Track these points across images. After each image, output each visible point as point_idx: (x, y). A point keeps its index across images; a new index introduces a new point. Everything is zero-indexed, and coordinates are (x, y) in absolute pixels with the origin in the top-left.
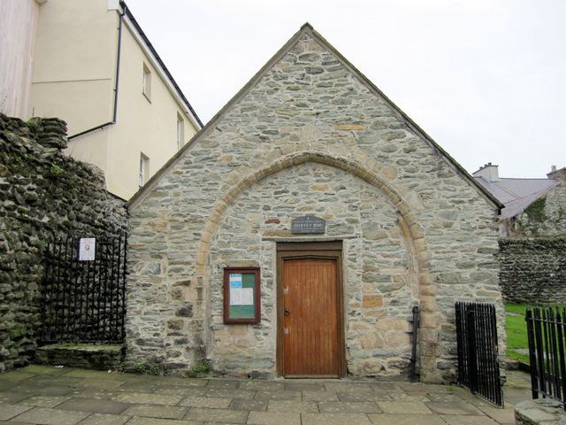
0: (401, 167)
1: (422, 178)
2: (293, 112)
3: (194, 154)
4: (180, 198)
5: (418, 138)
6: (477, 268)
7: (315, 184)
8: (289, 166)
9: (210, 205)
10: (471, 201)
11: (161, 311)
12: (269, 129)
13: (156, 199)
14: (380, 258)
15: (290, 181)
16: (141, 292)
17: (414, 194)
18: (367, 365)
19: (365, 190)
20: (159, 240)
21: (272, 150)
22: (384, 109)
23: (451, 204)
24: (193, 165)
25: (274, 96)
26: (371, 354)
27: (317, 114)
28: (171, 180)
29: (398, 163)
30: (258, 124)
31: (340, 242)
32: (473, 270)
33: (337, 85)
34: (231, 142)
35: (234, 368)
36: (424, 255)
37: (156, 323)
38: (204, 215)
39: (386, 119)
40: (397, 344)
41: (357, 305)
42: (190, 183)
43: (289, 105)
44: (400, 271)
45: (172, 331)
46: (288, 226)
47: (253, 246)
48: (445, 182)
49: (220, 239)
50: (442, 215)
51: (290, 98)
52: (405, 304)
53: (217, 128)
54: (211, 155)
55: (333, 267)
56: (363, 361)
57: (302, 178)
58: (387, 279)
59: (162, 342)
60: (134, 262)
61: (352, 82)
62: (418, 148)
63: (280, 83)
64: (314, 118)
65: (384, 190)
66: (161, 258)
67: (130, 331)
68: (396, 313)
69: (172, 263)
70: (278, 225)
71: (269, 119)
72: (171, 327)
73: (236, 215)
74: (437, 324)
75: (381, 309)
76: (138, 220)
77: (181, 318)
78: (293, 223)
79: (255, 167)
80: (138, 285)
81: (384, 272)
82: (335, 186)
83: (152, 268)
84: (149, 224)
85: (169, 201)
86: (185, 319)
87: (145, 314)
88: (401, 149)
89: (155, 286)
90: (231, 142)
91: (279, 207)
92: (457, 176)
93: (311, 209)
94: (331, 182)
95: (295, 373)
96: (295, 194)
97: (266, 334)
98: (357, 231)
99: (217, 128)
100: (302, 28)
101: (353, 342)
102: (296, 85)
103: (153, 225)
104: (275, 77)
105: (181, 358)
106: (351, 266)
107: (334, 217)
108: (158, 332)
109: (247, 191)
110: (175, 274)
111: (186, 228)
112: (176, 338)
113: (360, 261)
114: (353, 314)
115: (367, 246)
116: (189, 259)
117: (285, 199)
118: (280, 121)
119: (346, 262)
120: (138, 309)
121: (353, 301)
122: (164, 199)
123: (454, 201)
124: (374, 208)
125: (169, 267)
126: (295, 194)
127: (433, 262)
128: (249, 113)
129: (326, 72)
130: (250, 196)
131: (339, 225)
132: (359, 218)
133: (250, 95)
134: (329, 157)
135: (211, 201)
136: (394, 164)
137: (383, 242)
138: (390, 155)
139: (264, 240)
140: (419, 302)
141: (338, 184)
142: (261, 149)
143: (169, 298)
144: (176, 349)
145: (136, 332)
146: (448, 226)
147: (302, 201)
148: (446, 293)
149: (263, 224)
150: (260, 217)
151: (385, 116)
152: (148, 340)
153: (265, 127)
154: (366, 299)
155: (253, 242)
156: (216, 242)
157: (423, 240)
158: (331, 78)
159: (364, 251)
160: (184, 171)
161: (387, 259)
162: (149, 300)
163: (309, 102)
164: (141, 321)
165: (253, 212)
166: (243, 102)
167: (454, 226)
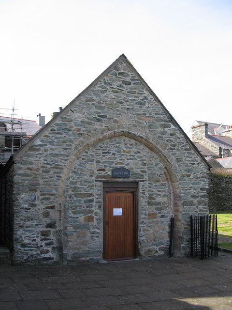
1: (177, 150)
3: (57, 125)
10: (198, 164)
11: (36, 225)
12: (102, 114)
14: (156, 192)
25: (105, 95)
29: (167, 141)
31: (137, 183)
32: (198, 199)
33: (139, 93)
34: (80, 120)
39: (162, 116)
40: (163, 238)
41: (145, 218)
44: (165, 199)
45: (43, 237)
46: (110, 173)
49: (71, 179)
54: (67, 127)
57: (117, 145)
58: (159, 204)
63: (108, 87)
64: (126, 111)
67: (16, 239)
69: (44, 194)
71: (102, 108)
76: (20, 165)
77: (49, 229)
78: (113, 171)
81: (158, 199)
91: (106, 162)
93: (122, 163)
97: (97, 237)
98: (146, 177)
104: (105, 83)
105: (50, 254)
108: (35, 238)
110: (45, 202)
111: (51, 172)
112: (46, 241)
113: (147, 194)
115: (151, 186)
116: (54, 192)
117: (109, 157)
119: (140, 195)
121: (143, 216)
123: (191, 163)
127: (182, 195)
128: (90, 103)
137: (158, 184)
138: (164, 136)
139: (96, 181)
142: (97, 126)
144: (46, 248)
146: (188, 176)
147: (118, 159)
149: (96, 171)
150: (94, 167)
152: (28, 244)
154: (150, 215)
157: (177, 183)
158: (135, 89)
160: (51, 135)
161: (160, 193)
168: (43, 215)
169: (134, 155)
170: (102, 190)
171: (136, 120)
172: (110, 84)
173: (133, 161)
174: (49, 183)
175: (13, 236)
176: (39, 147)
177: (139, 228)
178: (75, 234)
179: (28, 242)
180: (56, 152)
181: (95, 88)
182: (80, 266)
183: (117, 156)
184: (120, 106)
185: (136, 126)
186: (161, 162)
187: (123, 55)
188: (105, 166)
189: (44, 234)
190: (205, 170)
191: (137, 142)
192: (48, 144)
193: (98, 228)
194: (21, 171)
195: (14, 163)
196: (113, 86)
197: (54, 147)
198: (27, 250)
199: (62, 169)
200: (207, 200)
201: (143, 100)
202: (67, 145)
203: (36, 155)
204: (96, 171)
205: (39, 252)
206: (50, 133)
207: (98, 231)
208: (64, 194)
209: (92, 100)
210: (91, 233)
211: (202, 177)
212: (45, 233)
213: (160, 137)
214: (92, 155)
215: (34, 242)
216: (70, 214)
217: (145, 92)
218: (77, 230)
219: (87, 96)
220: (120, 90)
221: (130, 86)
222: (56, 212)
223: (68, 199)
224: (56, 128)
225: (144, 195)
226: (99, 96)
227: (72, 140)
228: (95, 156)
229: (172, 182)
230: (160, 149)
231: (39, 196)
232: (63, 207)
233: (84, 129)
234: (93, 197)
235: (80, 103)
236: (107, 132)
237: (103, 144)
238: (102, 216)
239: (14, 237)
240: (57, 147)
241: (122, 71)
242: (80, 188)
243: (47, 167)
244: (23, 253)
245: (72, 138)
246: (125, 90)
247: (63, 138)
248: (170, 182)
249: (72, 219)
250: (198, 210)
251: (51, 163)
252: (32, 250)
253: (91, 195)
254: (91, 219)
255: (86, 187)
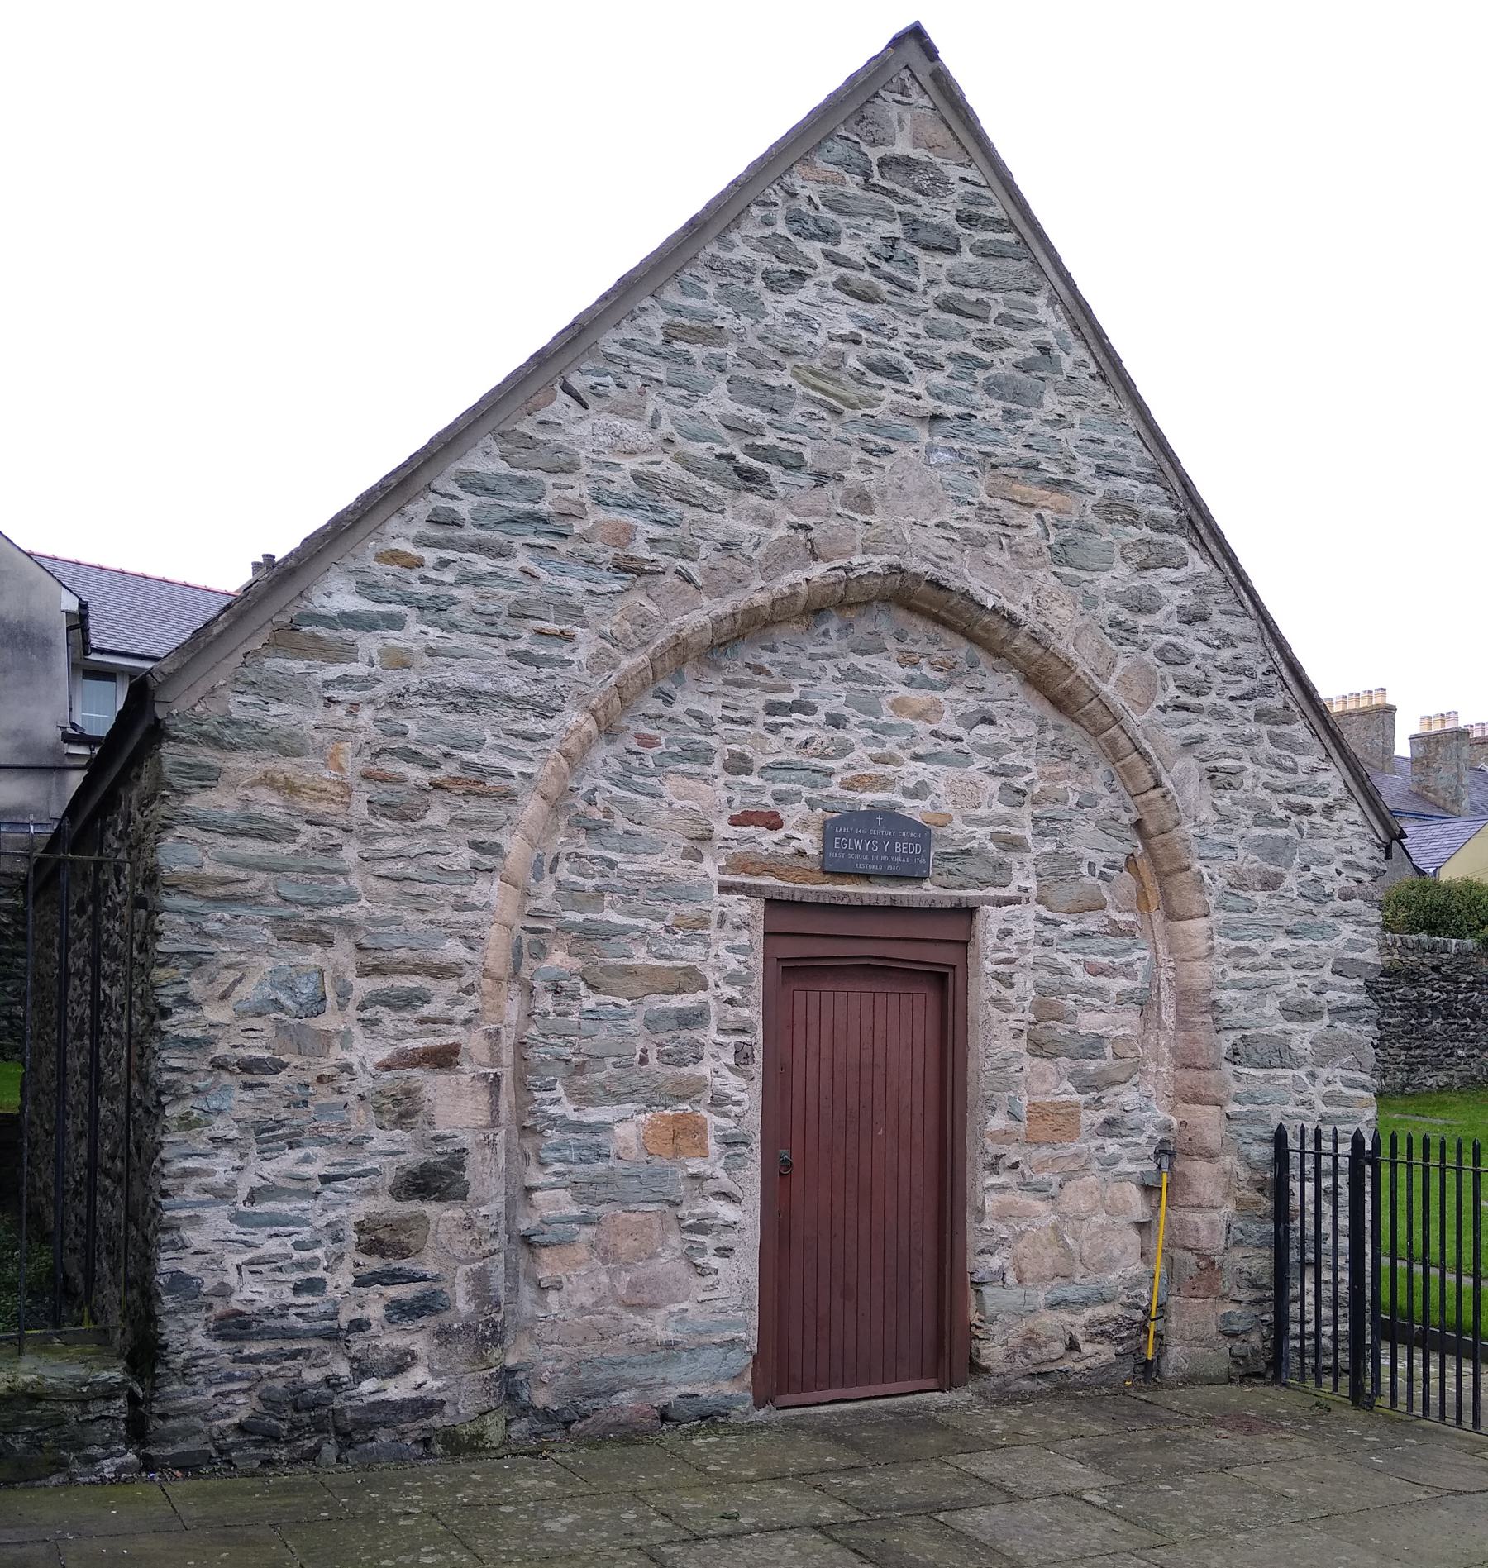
0: (1166, 670)
1: (1217, 714)
2: (854, 392)
3: (472, 484)
4: (413, 679)
5: (1218, 577)
6: (1327, 1019)
7: (903, 691)
8: (815, 609)
9: (541, 727)
10: (1328, 810)
11: (326, 1179)
12: (770, 439)
13: (298, 666)
14: (1080, 976)
15: (823, 670)
16: (238, 1103)
17: (1187, 765)
18: (1031, 1340)
19: (1050, 735)
20: (316, 860)
21: (781, 531)
22: (1136, 455)
23: (1281, 814)
24: (470, 532)
25: (790, 302)
26: (1041, 1298)
27: (936, 418)
28: (367, 588)
29: (1161, 654)
30: (732, 408)
31: (967, 912)
32: (1317, 1027)
33: (1003, 320)
34: (630, 464)
35: (612, 1392)
36: (1200, 974)
37: (306, 1234)
38: (517, 767)
39: (1140, 489)
40: (1111, 1262)
41: (1006, 1136)
42: (456, 614)
43: (842, 357)
44: (1126, 1024)
45: (374, 1264)
46: (809, 840)
47: (687, 909)
48: (1275, 740)
49: (564, 872)
50: (1258, 846)
51: (847, 327)
52: (1138, 1129)
53: (567, 389)
54: (544, 507)
55: (932, 996)
56: (1022, 1327)
57: (860, 662)
58: (1095, 1046)
59: (334, 1316)
60: (196, 961)
61: (1052, 322)
62: (1216, 616)
63: (812, 249)
64: (922, 434)
65: (1112, 743)
66: (326, 942)
67: (180, 1281)
68: (1114, 1161)
69: (378, 970)
70: (778, 835)
71: (772, 400)
72: (373, 1247)
73: (622, 781)
74: (1226, 1195)
75: (1075, 1148)
76: (208, 756)
77: (414, 1206)
78: (828, 832)
79: (718, 592)
80: (219, 1065)
81: (1090, 1022)
82: (962, 708)
83: (290, 988)
84: (268, 781)
85: (365, 683)
86: (431, 1209)
87: (252, 1198)
88: (1171, 607)
89: (298, 1068)
90: (630, 464)
91: (786, 767)
92: (1299, 724)
93: (885, 784)
94: (953, 693)
95: (804, 1388)
96: (836, 721)
97: (724, 1252)
98: (1022, 879)
99: (567, 389)
100: (897, 42)
101: (995, 1262)
102: (866, 276)
103: (289, 788)
104: (795, 218)
105: (418, 1374)
106: (998, 1002)
107: (957, 822)
108: (318, 1273)
109: (666, 685)
110: (390, 1020)
111: (437, 816)
112: (394, 1292)
113: (1025, 983)
114: (993, 1168)
115: (1047, 934)
116: (454, 951)
117: (801, 735)
118: (811, 416)
119: (982, 990)
120: (220, 1179)
121: (997, 1122)
122: (335, 671)
123: (1291, 807)
124: (1074, 799)
125: (363, 987)
126: (836, 721)
127: (1224, 997)
128: (697, 352)
129: (968, 257)
130: (677, 709)
131: (967, 853)
132: (1027, 833)
133: (703, 272)
134: (966, 595)
135: (545, 712)
136: (1149, 656)
137: (1091, 923)
138: (1143, 621)
139: (725, 888)
140: (1175, 1122)
141: (972, 703)
142: (736, 518)
143: (361, 1119)
144: (393, 1340)
145: (210, 1283)
146: (1270, 883)
147: (860, 753)
148: (1252, 1098)
149: (722, 829)
150: (713, 795)
151: (1138, 477)
152: (268, 1313)
153: (758, 430)
154: (1038, 1112)
155: (687, 895)
156: (548, 888)
157: (1202, 923)
158: (984, 286)
159: (1037, 951)
160: (430, 556)
161: (1100, 981)
162: (270, 1135)
163: (908, 364)
164: (234, 1231)
165: (690, 776)
166: (671, 295)
167: (1286, 883)
168: (379, 1111)
169: (959, 731)
170: (759, 948)
171: (985, 498)
172: (829, 235)
173: (952, 772)
174: (420, 888)
175: (150, 1261)
176: (348, 634)
177: (974, 1196)
178: (587, 1233)
179: (266, 1302)
180: (463, 676)
181: (731, 246)
182: (573, 1429)
183: (854, 734)
184: (888, 395)
185: (981, 542)
186: (1117, 785)
187: (916, 33)
188: (780, 798)
189: (377, 1239)
190: (1366, 853)
191: (980, 654)
192: (412, 614)
193: (726, 1196)
194: (212, 796)
195: (158, 732)
196: (844, 248)
197: (455, 640)
198: (252, 1359)
199: (507, 796)
200: (1364, 1034)
201: (1025, 366)
202: (539, 633)
203: (327, 684)
204: (722, 829)
205: (342, 1369)
206: (423, 541)
207: (727, 1212)
208: (517, 965)
209: (712, 334)
210: (691, 1229)
211: (1347, 896)
212: (384, 1234)
213: (1119, 624)
214: (698, 717)
215: (306, 1299)
216: (556, 1101)
217: (1045, 314)
218: (598, 1210)
219: (671, 295)
220: (891, 279)
221: (948, 262)
222: (454, 1106)
223: (546, 1002)
224: (465, 506)
225: (1007, 993)
226: (751, 306)
227: (576, 600)
228: (720, 728)
229: (1171, 916)
230: (1118, 701)
231: (350, 977)
232: (507, 1057)
233: (657, 531)
234: (702, 996)
235: (625, 344)
236: (802, 566)
237: (773, 650)
238: (756, 1118)
239: (165, 1265)
240: (475, 643)
241: (902, 147)
242: (624, 931)
243: (401, 781)
244: (231, 1378)
245: (570, 583)
246: (919, 282)
247: (512, 583)
248: (1158, 917)
249: (570, 1136)
250: (1316, 1091)
251: (433, 752)
252: (294, 1355)
253: (692, 979)
254: (686, 1133)
255: (656, 926)
